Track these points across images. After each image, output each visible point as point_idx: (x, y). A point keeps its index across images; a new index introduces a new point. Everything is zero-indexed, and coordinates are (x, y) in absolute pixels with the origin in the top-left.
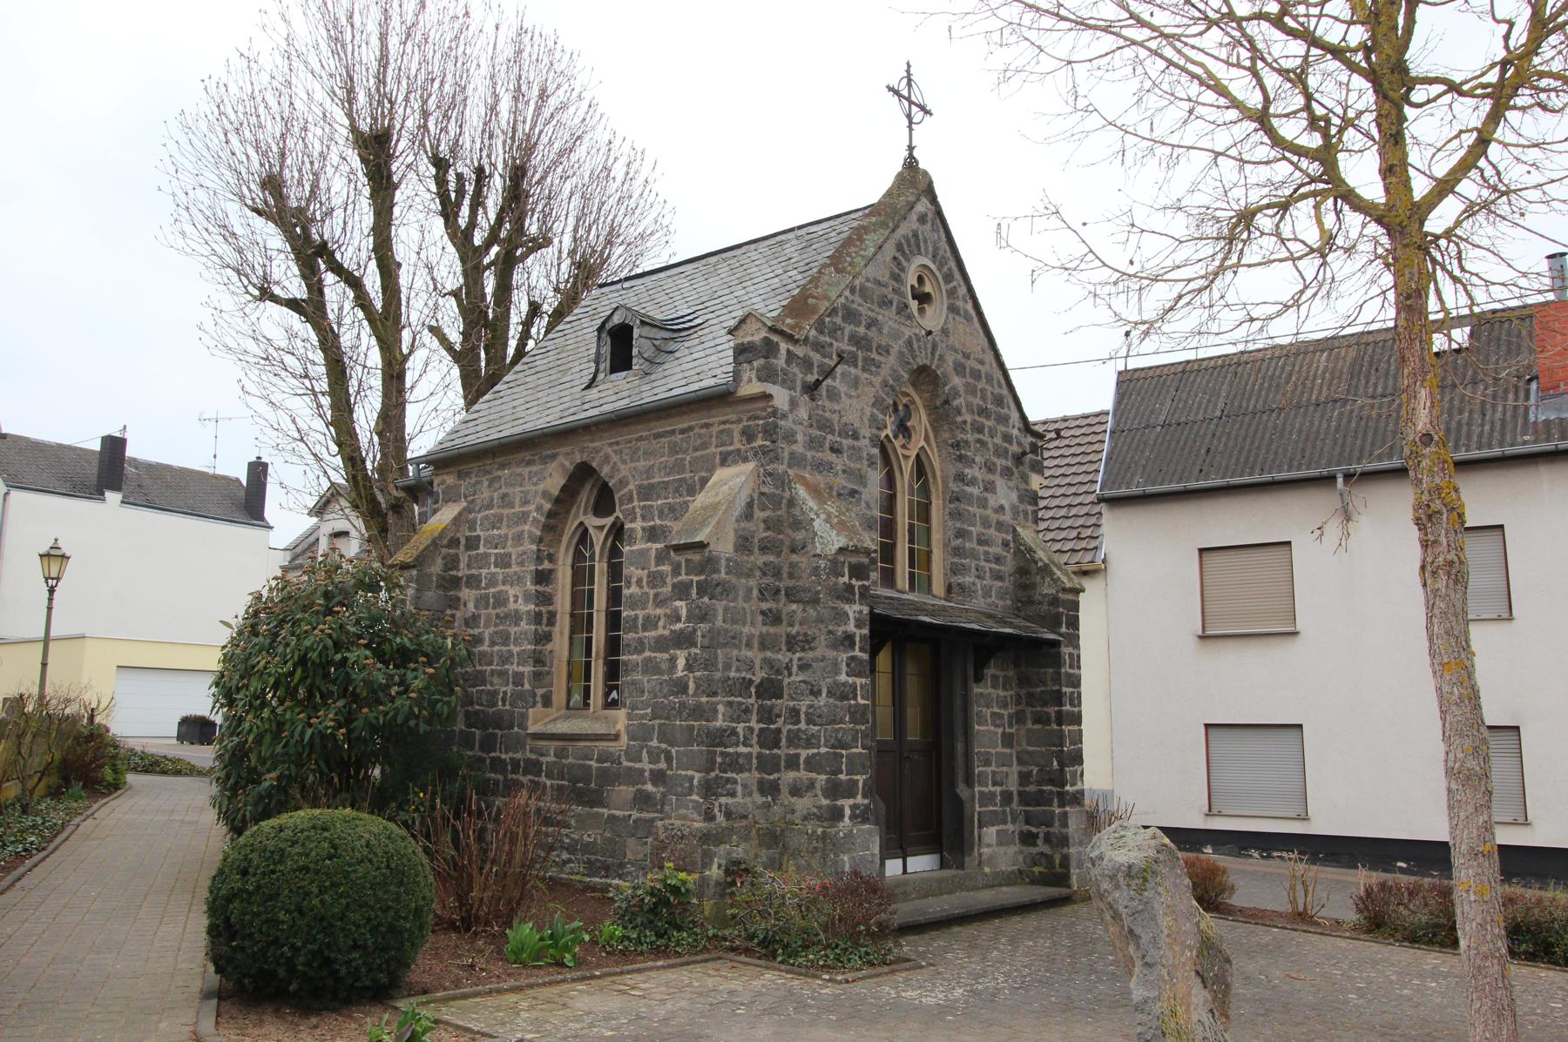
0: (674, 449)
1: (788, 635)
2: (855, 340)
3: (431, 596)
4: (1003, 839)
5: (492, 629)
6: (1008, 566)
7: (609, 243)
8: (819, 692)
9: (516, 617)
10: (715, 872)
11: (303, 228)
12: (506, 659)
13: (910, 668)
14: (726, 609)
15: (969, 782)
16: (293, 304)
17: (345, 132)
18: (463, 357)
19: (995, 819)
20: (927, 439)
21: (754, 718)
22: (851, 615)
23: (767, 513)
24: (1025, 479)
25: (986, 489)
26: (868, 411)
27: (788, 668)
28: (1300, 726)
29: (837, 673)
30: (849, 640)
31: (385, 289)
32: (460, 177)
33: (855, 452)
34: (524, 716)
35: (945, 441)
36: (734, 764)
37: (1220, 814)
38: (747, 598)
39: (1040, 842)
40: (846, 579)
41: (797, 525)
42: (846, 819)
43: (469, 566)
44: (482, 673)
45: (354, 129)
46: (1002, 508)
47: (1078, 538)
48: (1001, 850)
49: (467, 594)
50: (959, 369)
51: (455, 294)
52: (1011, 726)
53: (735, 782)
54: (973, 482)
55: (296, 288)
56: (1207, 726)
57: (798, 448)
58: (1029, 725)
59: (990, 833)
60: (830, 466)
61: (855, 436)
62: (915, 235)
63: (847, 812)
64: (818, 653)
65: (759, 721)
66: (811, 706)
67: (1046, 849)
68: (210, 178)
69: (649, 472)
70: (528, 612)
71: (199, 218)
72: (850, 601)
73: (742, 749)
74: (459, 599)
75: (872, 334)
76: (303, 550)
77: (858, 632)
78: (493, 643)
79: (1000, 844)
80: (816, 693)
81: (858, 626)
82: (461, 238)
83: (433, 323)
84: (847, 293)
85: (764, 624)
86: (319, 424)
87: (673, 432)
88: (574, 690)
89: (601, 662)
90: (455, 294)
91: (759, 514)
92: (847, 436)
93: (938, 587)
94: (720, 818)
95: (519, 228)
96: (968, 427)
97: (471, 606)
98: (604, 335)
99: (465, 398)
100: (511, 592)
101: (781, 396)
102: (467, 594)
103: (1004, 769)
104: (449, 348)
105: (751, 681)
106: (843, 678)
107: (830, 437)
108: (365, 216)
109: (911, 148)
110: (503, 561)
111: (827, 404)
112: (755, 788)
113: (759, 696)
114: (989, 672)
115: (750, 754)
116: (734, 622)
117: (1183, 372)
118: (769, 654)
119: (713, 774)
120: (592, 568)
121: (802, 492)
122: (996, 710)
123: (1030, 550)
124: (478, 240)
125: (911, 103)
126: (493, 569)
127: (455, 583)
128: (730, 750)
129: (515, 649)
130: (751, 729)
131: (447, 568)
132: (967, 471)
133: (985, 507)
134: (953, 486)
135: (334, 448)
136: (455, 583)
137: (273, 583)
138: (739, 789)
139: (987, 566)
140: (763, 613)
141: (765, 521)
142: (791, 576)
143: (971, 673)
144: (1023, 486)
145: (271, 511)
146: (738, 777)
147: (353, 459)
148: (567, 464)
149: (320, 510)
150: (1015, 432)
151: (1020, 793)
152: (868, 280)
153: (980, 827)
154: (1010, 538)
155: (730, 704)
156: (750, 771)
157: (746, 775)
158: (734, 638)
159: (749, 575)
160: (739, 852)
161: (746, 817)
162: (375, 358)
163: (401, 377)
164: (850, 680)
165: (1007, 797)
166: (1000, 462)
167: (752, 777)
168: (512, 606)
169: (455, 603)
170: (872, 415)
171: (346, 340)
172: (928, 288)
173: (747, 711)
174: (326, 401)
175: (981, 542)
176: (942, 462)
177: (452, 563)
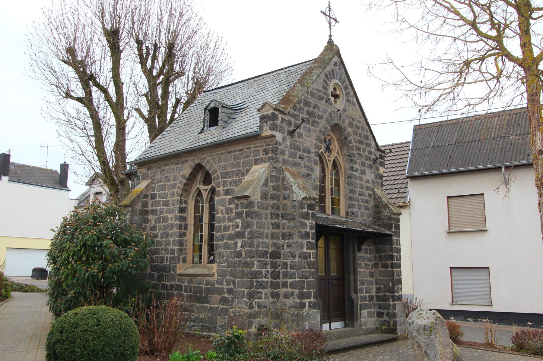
0: (236, 158)
1: (282, 233)
2: (309, 113)
3: (137, 218)
4: (370, 315)
5: (162, 231)
6: (371, 204)
8: (295, 256)
9: (171, 227)
13: (332, 246)
14: (257, 223)
15: (356, 292)
17: (100, 30)
18: (149, 121)
20: (338, 153)
21: (269, 267)
22: (308, 225)
24: (377, 169)
25: (362, 173)
26: (314, 141)
27: (283, 246)
29: (303, 248)
30: (307, 235)
32: (147, 48)
34: (175, 267)
36: (261, 285)
37: (456, 304)
38: (266, 218)
39: (385, 316)
40: (306, 210)
41: (286, 188)
42: (307, 307)
45: (104, 28)
46: (368, 181)
47: (398, 193)
48: (369, 319)
49: (151, 217)
50: (351, 125)
51: (146, 95)
52: (372, 269)
53: (262, 293)
54: (356, 170)
55: (81, 93)
56: (451, 268)
57: (286, 157)
58: (380, 269)
62: (333, 71)
63: (307, 305)
65: (271, 268)
66: (292, 262)
67: (387, 319)
69: (225, 167)
70: (176, 224)
72: (308, 219)
73: (264, 279)
74: (148, 219)
75: (316, 111)
76: (83, 200)
77: (311, 231)
78: (162, 237)
80: (294, 256)
81: (311, 229)
82: (148, 73)
83: (137, 107)
84: (305, 94)
85: (273, 228)
86: (90, 148)
87: (235, 151)
88: (195, 256)
89: (206, 245)
90: (146, 95)
91: (271, 184)
92: (306, 152)
93: (343, 213)
94: (256, 308)
96: (354, 148)
97: (153, 222)
98: (207, 112)
99: (150, 137)
101: (279, 136)
103: (370, 286)
104: (143, 117)
105: (268, 252)
106: (305, 250)
107: (299, 152)
108: (109, 64)
109: (330, 36)
110: (166, 204)
111: (298, 139)
112: (269, 295)
113: (271, 258)
114: (364, 247)
115: (268, 281)
116: (261, 228)
117: (440, 125)
118: (275, 241)
119: (252, 290)
121: (288, 175)
122: (366, 263)
123: (380, 198)
126: (162, 207)
127: (147, 213)
128: (259, 280)
129: (171, 240)
130: (268, 271)
131: (143, 207)
132: (354, 166)
133: (361, 180)
134: (349, 172)
135: (96, 158)
136: (147, 213)
138: (263, 296)
139: (363, 204)
141: (273, 187)
142: (283, 209)
143: (356, 247)
144: (376, 172)
146: (263, 291)
147: (104, 163)
148: (192, 164)
149: (90, 183)
150: (373, 150)
151: (376, 296)
152: (314, 89)
153: (361, 310)
154: (371, 193)
155: (259, 261)
156: (267, 288)
157: (266, 290)
158: (261, 234)
159: (267, 209)
160: (263, 322)
163: (124, 129)
164: (308, 251)
166: (367, 162)
167: (268, 291)
168: (170, 222)
169: (146, 221)
171: (101, 114)
172: (338, 92)
173: (266, 264)
174: (93, 139)
175: (360, 195)
176: (344, 162)
177: (145, 204)
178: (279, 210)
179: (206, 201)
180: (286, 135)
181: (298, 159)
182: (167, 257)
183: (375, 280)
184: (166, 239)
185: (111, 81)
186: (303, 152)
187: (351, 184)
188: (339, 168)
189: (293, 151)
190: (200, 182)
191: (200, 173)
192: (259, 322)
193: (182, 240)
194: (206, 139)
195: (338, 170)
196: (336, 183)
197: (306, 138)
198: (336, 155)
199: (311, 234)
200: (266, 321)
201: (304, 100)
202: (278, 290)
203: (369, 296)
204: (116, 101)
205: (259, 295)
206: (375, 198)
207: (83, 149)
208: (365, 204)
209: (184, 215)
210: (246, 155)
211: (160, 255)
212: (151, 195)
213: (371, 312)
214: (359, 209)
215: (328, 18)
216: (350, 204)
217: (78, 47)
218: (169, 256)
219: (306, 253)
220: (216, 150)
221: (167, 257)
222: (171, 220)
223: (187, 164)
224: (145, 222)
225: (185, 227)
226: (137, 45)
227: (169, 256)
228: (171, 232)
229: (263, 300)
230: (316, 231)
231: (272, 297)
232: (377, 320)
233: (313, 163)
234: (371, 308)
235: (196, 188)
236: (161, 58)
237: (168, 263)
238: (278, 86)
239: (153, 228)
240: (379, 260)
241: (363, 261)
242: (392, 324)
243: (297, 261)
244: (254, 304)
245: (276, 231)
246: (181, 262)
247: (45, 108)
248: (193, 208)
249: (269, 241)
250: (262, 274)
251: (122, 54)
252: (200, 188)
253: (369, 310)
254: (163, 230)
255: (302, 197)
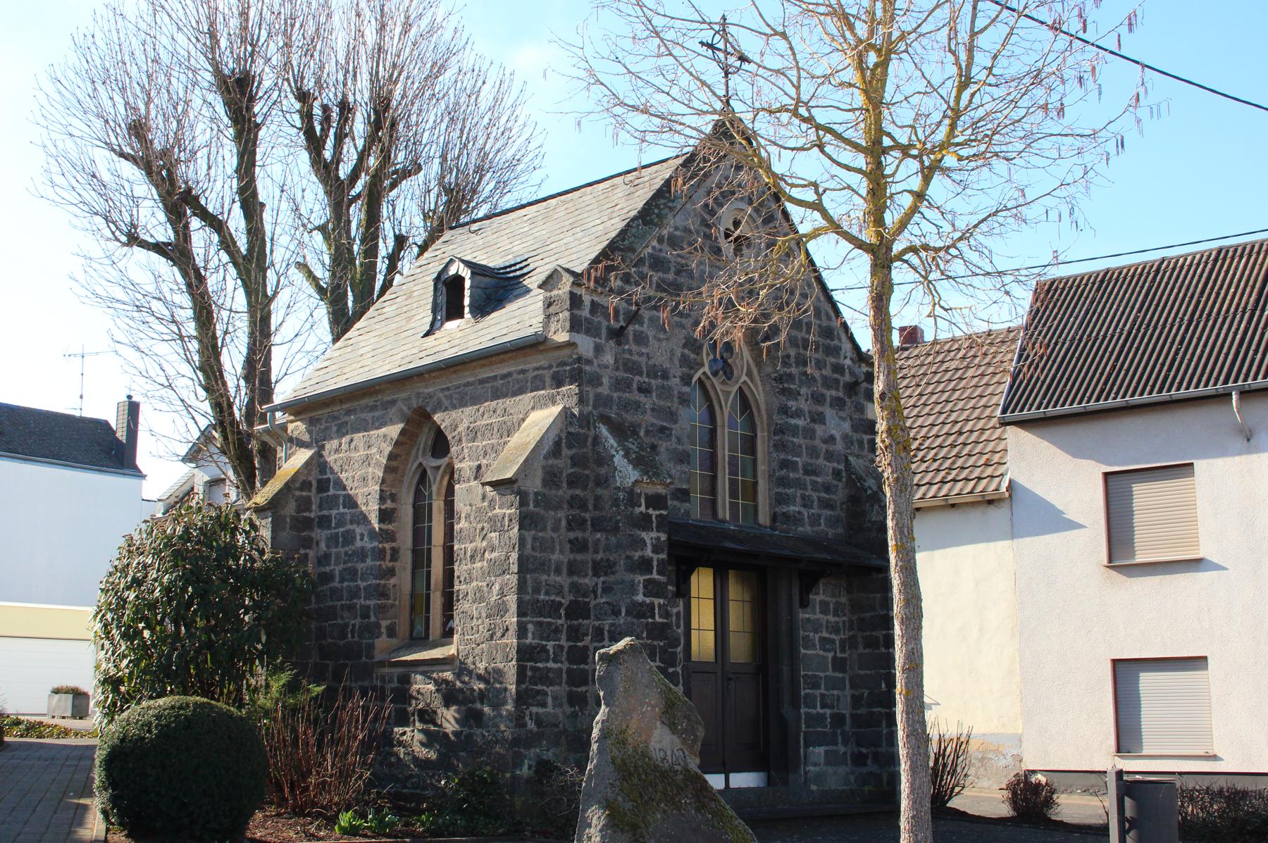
1: (594, 561)
4: (831, 759)
5: (341, 567)
6: (840, 495)
7: (480, 170)
8: (619, 612)
9: (362, 555)
10: (525, 771)
11: (168, 170)
12: (354, 594)
13: (735, 591)
14: (535, 539)
15: (795, 704)
16: (158, 248)
17: (209, 76)
18: (332, 295)
19: (821, 740)
20: (749, 374)
21: (564, 637)
22: (648, 542)
23: (574, 451)
25: (813, 421)
26: (678, 352)
27: (594, 592)
28: (1205, 658)
29: (634, 592)
30: (645, 565)
31: (249, 232)
32: (325, 109)
33: (666, 392)
34: (371, 647)
35: (768, 375)
36: (544, 677)
38: (556, 529)
39: (869, 762)
40: (643, 509)
43: (321, 507)
44: (334, 608)
45: (217, 72)
46: (832, 439)
48: (830, 769)
49: (320, 535)
51: (322, 229)
52: (843, 650)
53: (546, 694)
54: (798, 414)
55: (164, 233)
57: (604, 390)
58: (861, 650)
59: (819, 751)
60: (638, 406)
61: (665, 376)
64: (618, 577)
65: (568, 640)
66: (612, 625)
68: (78, 126)
70: (373, 549)
71: (67, 166)
73: (551, 665)
74: (311, 539)
76: (180, 501)
77: (655, 557)
78: (342, 580)
79: (829, 762)
81: (655, 551)
82: (325, 170)
83: (300, 260)
85: (572, 551)
86: (187, 369)
87: (495, 378)
88: (417, 621)
89: (439, 594)
90: (322, 229)
91: (566, 452)
92: (656, 377)
94: (531, 725)
95: (386, 158)
97: (323, 546)
98: (440, 286)
99: (332, 332)
100: (358, 531)
102: (320, 535)
103: (836, 692)
105: (560, 604)
106: (640, 598)
107: (637, 378)
108: (229, 156)
111: (634, 348)
112: (565, 700)
113: (568, 617)
114: (818, 597)
115: (561, 669)
118: (575, 578)
119: (524, 686)
120: (430, 505)
121: (604, 430)
122: (825, 635)
123: (860, 479)
124: (344, 171)
125: (727, 53)
126: (342, 510)
128: (540, 665)
129: (362, 584)
130: (561, 647)
131: (299, 510)
132: (790, 403)
133: (813, 437)
134: (777, 419)
135: (202, 393)
136: (307, 524)
137: (144, 526)
138: (550, 700)
139: (815, 495)
140: (570, 541)
141: (572, 458)
142: (596, 508)
143: (796, 598)
145: (142, 460)
146: (549, 690)
147: (221, 406)
148: (405, 409)
149: (193, 456)
150: (848, 362)
151: (852, 716)
152: (676, 228)
153: (806, 747)
154: (842, 467)
155: (540, 624)
156: (560, 684)
157: (557, 688)
158: (543, 564)
159: (558, 507)
160: (549, 755)
161: (557, 726)
162: (240, 301)
163: (266, 319)
164: (648, 600)
165: (838, 720)
166: (830, 393)
167: (562, 689)
168: (358, 544)
169: (308, 543)
170: (683, 355)
171: (212, 282)
173: (557, 630)
174: (194, 346)
175: (807, 472)
177: (304, 504)
178: (586, 510)
179: (438, 494)
180: (603, 341)
181: (636, 392)
182: (354, 625)
183: (851, 678)
184: (352, 584)
185: (234, 202)
186: (648, 376)
187: (784, 446)
188: (754, 410)
189: (621, 374)
190: (425, 449)
191: (426, 430)
192: (538, 756)
193: (385, 585)
194: (436, 350)
195: (751, 414)
196: (750, 445)
197: (656, 344)
198: (744, 378)
199: (655, 563)
200: (554, 754)
201: (650, 255)
202: (583, 689)
203: (832, 716)
204: (248, 250)
205: (539, 698)
206: (849, 479)
207: (171, 371)
208: (823, 495)
209: (390, 527)
210: (517, 386)
211: (340, 621)
212: (319, 481)
213: (836, 752)
214: (805, 506)
215: (730, 49)
216: (781, 494)
217: (156, 121)
218: (358, 621)
219: (642, 604)
220: (454, 376)
221: (354, 625)
222: (362, 539)
223: (394, 410)
224: (305, 547)
225: (392, 555)
226: (298, 106)
227: (358, 621)
228: (360, 566)
229: (550, 709)
230: (669, 555)
231: (571, 704)
232: (853, 773)
233: (676, 400)
234: (836, 744)
235: (416, 465)
236: (359, 126)
237: (356, 639)
238: (605, 218)
239: (323, 559)
240: (859, 630)
241: (816, 631)
242: (885, 779)
243: (622, 621)
244: (527, 718)
245: (579, 557)
246: (384, 636)
247: (81, 276)
248: (410, 510)
249: (563, 580)
250: (547, 652)
251: (261, 133)
252: (424, 463)
253: (830, 748)
254: (345, 562)
255: (633, 480)
